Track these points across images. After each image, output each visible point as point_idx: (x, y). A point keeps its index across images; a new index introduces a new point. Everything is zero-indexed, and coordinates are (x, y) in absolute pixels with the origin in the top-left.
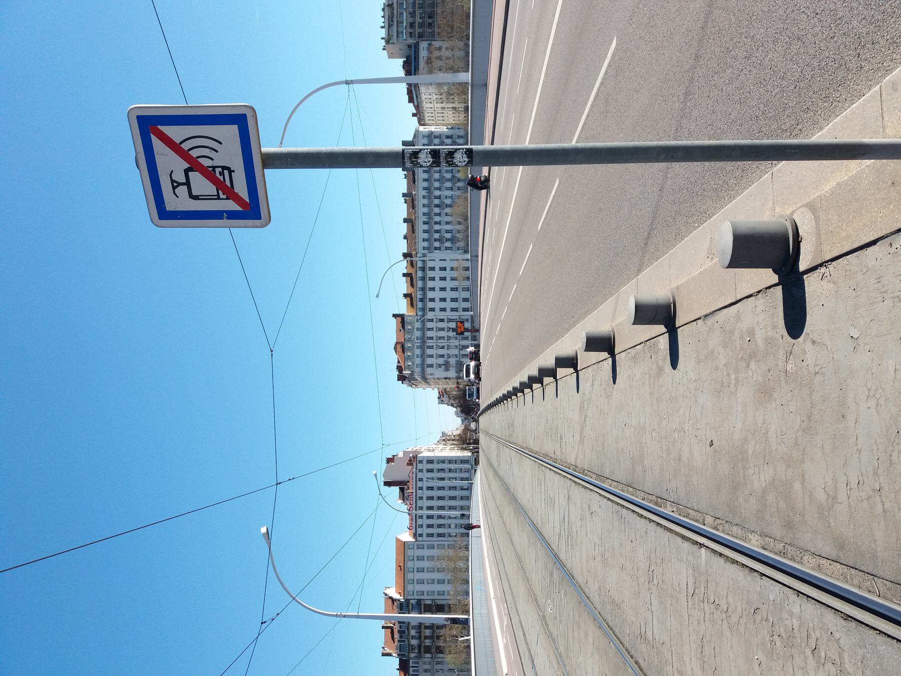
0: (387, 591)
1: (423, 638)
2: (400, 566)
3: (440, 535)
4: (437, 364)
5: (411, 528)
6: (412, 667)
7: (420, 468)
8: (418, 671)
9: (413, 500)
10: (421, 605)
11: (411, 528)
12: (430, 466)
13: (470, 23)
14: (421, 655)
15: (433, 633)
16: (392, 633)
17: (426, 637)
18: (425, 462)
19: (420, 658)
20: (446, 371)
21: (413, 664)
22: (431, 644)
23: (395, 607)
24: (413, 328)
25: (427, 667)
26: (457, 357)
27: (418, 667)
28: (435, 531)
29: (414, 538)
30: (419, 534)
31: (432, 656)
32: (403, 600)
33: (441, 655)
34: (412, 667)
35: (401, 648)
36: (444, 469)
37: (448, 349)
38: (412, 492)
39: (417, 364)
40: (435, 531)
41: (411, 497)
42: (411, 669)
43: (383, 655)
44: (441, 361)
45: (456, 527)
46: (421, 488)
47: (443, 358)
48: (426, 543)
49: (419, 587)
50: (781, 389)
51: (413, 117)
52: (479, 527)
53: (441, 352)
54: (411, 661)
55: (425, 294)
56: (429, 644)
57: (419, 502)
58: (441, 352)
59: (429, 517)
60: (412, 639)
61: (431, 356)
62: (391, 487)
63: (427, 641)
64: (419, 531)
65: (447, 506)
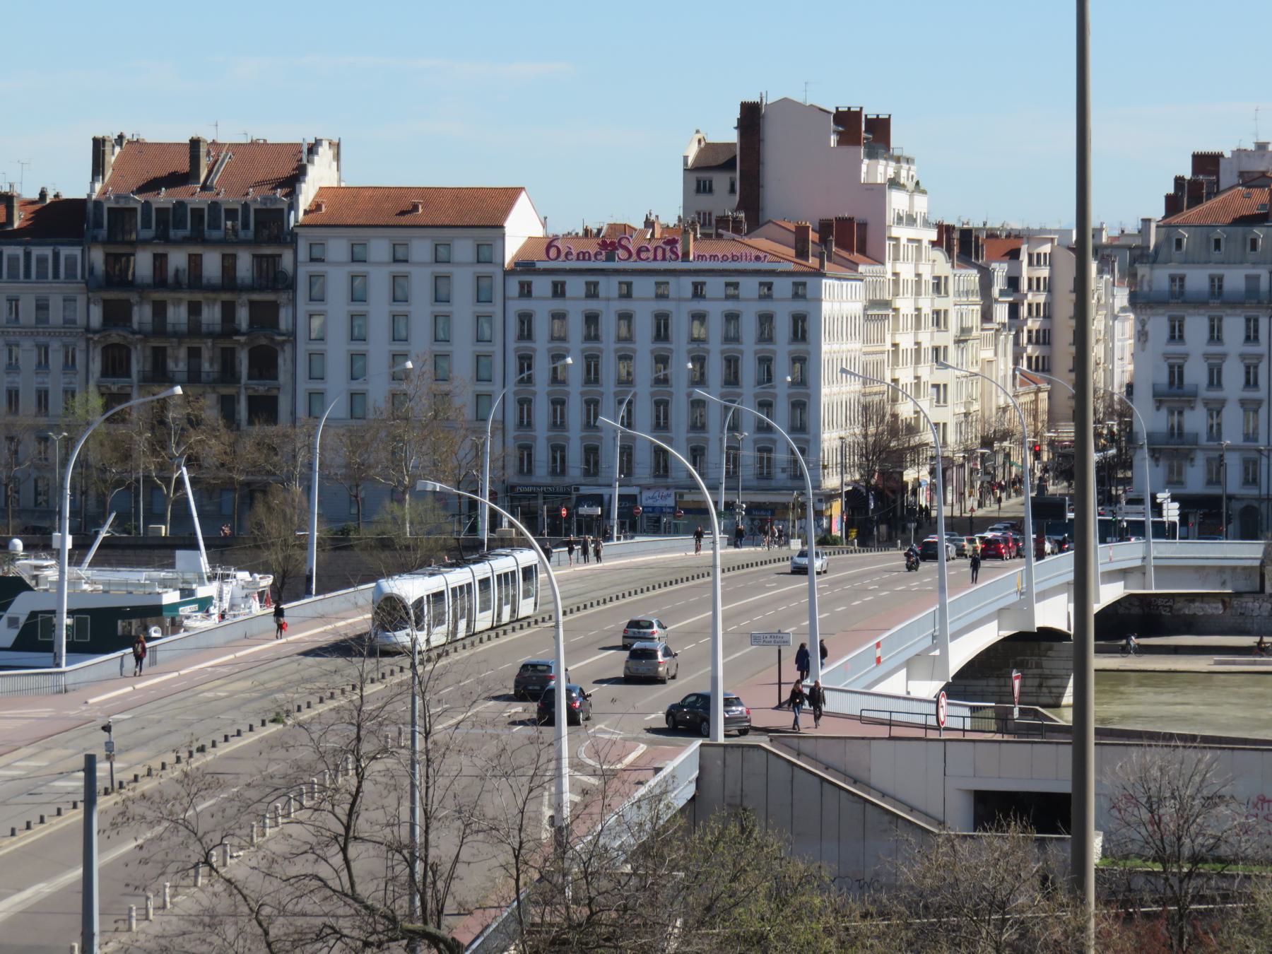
0: (325, 152)
1: (157, 296)
2: (415, 208)
3: (526, 362)
4: (1185, 356)
5: (553, 252)
6: (56, 256)
8: (42, 275)
9: (655, 259)
10: (275, 289)
11: (553, 252)
12: (783, 328)
14: (100, 288)
15: (176, 334)
16: (175, 180)
17: (160, 309)
18: (799, 306)
19: (87, 284)
20: (1154, 396)
21: (67, 258)
22: (135, 326)
23: (266, 191)
24: (1186, 262)
25: (56, 315)
26: (1210, 438)
27: (56, 275)
28: (749, 349)
29: (517, 264)
30: (563, 284)
31: (95, 332)
32: (292, 224)
33: (96, 366)
34: (56, 256)
35: (120, 216)
36: (769, 380)
37: (1243, 403)
38: (686, 255)
41: (668, 254)
42: (48, 251)
43: (99, 144)
44: (1196, 374)
46: (698, 291)
48: (497, 309)
49: (337, 281)
50: (217, 872)
52: (697, 549)
53: (1233, 374)
54: (77, 251)
55: (1198, 303)
56: (135, 318)
57: (687, 282)
58: (1233, 374)
59: (766, 320)
61: (1215, 336)
64: (542, 286)
65: (671, 394)
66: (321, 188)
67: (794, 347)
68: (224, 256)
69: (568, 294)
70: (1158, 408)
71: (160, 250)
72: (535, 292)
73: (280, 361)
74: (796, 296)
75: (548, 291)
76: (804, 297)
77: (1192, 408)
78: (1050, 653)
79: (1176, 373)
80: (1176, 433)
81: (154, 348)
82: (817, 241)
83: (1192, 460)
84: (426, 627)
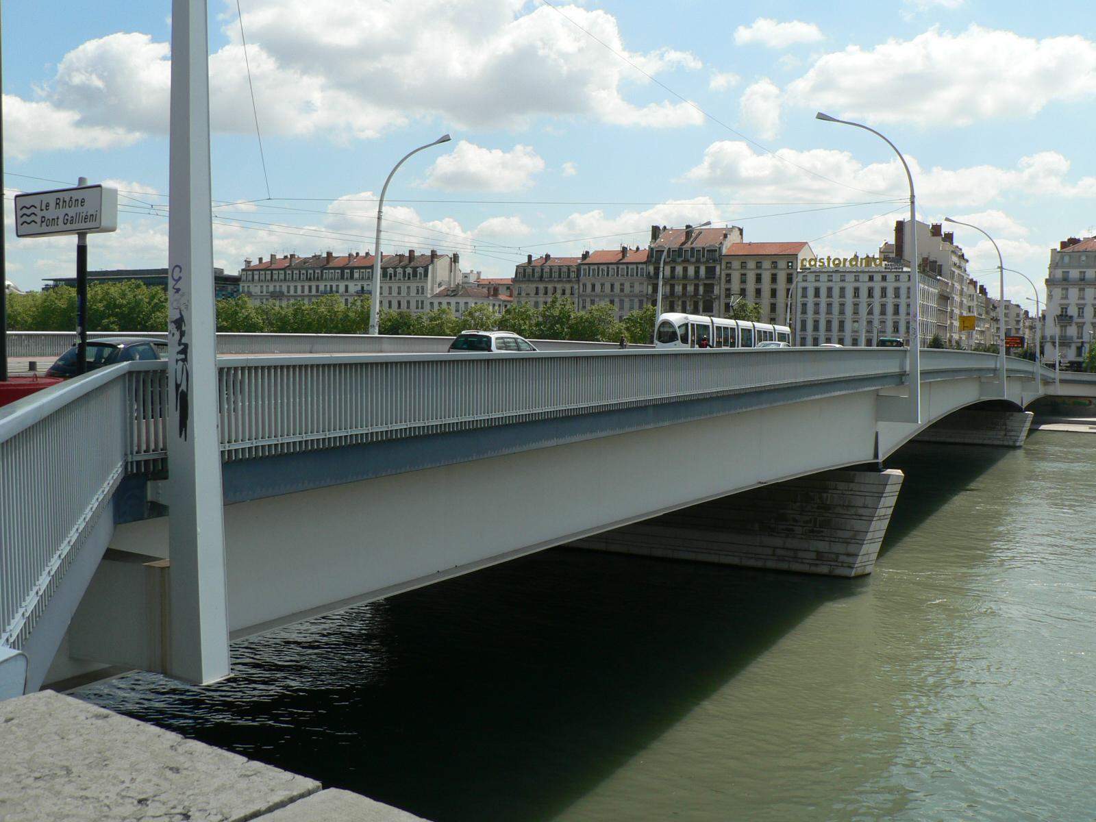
4: (1068, 305)
7: (901, 277)
13: (240, 332)
18: (909, 284)
25: (627, 289)
26: (642, 300)
27: (637, 275)
39: (1068, 272)
40: (811, 299)
44: (1072, 311)
45: (855, 331)
47: (1077, 314)
59: (857, 290)
62: (894, 232)
63: (681, 287)
66: (517, 266)
67: (868, 300)
68: (695, 267)
71: (673, 265)
73: (714, 305)
75: (880, 278)
77: (1071, 326)
78: (1011, 418)
79: (1064, 309)
81: (670, 301)
83: (1070, 346)
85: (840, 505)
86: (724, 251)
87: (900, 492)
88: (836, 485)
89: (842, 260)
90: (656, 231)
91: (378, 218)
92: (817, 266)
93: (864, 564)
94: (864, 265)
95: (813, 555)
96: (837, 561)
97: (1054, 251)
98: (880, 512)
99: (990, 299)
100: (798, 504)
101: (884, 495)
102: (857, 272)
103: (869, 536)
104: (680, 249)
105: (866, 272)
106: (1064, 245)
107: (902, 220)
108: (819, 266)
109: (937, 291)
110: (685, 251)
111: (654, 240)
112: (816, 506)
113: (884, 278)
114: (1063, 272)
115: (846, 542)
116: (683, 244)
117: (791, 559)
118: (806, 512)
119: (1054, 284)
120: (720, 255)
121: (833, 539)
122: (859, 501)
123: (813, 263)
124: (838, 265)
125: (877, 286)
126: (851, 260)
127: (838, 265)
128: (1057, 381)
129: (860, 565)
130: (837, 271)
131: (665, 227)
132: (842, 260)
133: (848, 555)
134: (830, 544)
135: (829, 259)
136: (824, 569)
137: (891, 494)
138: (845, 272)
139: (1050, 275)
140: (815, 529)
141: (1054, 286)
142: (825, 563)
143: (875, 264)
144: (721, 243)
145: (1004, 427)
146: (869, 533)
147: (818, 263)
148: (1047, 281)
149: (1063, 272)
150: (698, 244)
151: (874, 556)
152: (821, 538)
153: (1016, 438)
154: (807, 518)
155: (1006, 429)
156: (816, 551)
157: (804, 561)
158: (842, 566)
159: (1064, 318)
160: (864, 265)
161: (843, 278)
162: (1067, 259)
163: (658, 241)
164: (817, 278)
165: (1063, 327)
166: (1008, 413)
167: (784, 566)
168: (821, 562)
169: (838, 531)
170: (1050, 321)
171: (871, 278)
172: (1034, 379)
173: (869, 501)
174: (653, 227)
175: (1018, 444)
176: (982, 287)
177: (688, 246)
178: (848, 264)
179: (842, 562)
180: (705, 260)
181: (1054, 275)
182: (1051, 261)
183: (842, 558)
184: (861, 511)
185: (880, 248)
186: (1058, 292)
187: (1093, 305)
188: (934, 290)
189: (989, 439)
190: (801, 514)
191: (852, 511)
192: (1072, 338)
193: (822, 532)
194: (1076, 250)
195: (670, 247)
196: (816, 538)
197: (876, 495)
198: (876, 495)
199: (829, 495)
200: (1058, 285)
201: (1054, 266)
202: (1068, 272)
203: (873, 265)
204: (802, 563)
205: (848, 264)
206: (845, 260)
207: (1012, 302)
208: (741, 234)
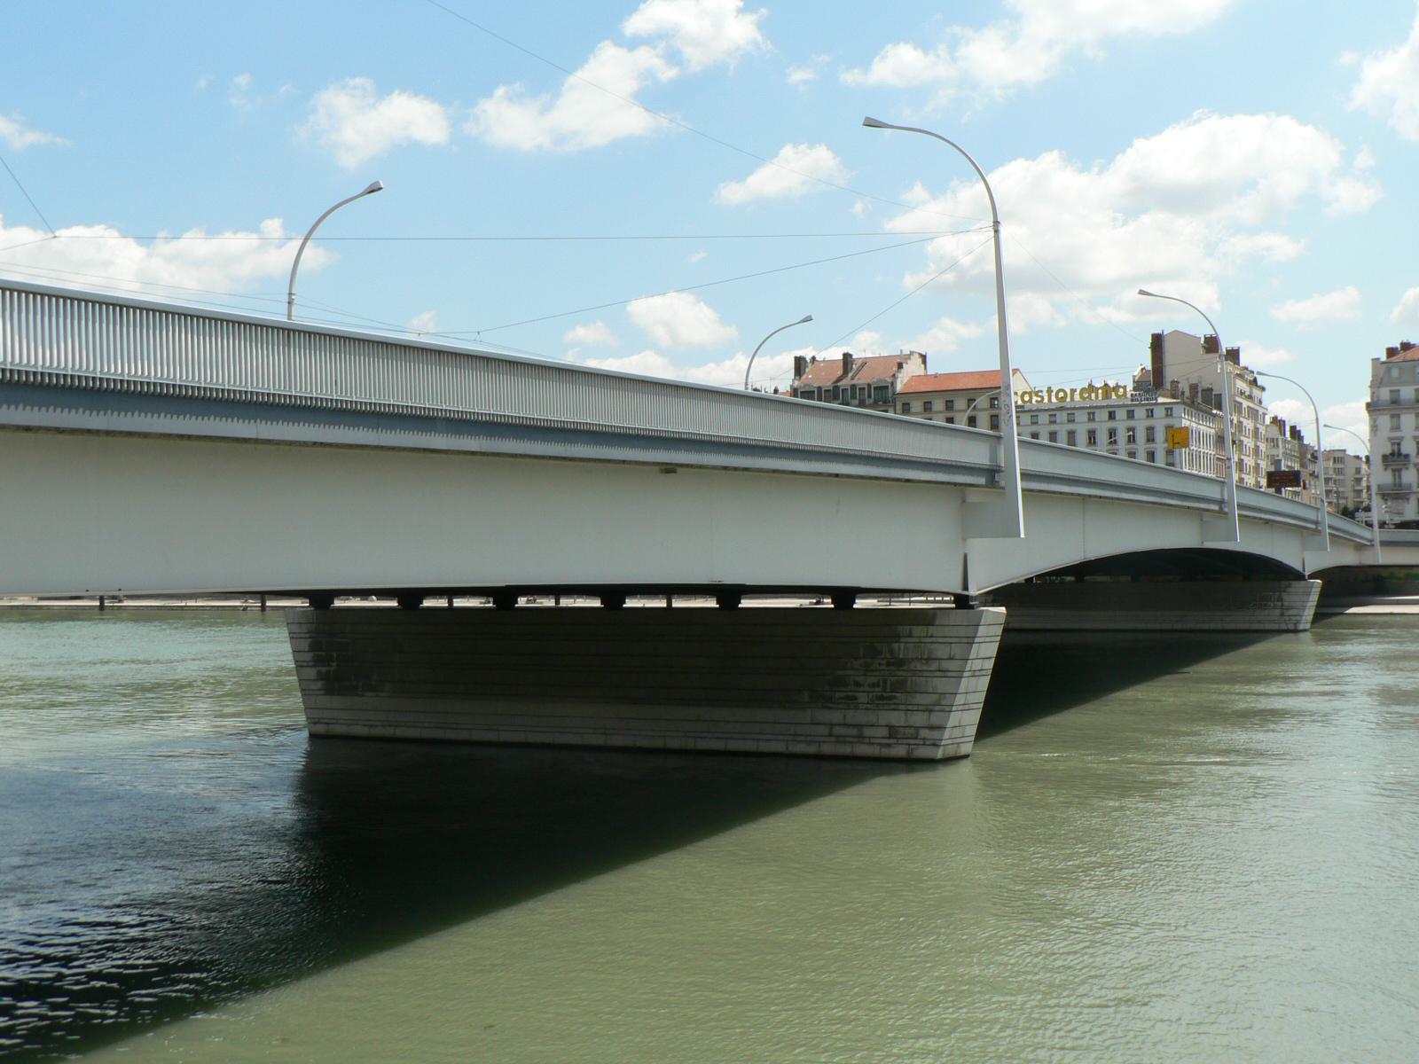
4: (1402, 438)
39: (1399, 391)
51: (793, 359)
57: (1064, 414)
60: (1068, 414)
62: (1150, 350)
69: (1174, 415)
70: (1386, 469)
72: (913, 410)
74: (992, 406)
76: (1037, 423)
77: (1407, 469)
78: (1289, 590)
80: (1398, 485)
82: (1136, 379)
83: (1408, 499)
84: (1137, 734)
85: (917, 658)
86: (899, 387)
87: (1002, 636)
88: (910, 630)
89: (1069, 392)
90: (800, 364)
91: (289, 303)
92: (1034, 402)
93: (955, 741)
94: (1100, 398)
95: (884, 732)
96: (916, 738)
97: (1375, 361)
98: (975, 664)
99: (1307, 446)
100: (861, 661)
101: (976, 640)
102: (1090, 407)
103: (960, 699)
104: (836, 388)
105: (1103, 407)
106: (1391, 352)
107: (1160, 332)
108: (1036, 401)
109: (1213, 431)
110: (843, 390)
111: (797, 378)
112: (884, 662)
113: (1131, 415)
114: (1391, 391)
115: (929, 710)
116: (839, 380)
117: (855, 740)
118: (873, 671)
119: (1379, 410)
120: (894, 394)
121: (910, 707)
122: (942, 651)
123: (1027, 398)
124: (1063, 399)
125: (1121, 425)
126: (1083, 390)
127: (1063, 399)
128: (1377, 543)
129: (950, 742)
130: (1062, 409)
131: (814, 358)
132: (1069, 392)
133: (932, 728)
134: (906, 715)
135: (1050, 391)
136: (900, 751)
137: (987, 639)
138: (1075, 408)
139: (1372, 397)
140: (885, 694)
141: (1378, 413)
142: (900, 741)
143: (1117, 395)
144: (894, 375)
145: (1280, 604)
146: (958, 695)
147: (1035, 399)
148: (1368, 405)
149: (1391, 391)
150: (861, 380)
151: (972, 730)
152: (893, 707)
153: (1298, 618)
154: (873, 680)
155: (1282, 606)
156: (887, 726)
157: (872, 741)
158: (924, 744)
159: (1395, 459)
160: (1100, 398)
161: (1071, 418)
162: (1395, 373)
163: (804, 377)
164: (1034, 420)
165: (1397, 472)
166: (1284, 583)
167: (845, 750)
168: (895, 741)
169: (918, 695)
170: (1377, 462)
171: (1112, 416)
172: (1317, 532)
173: (957, 650)
174: (796, 358)
175: (1301, 627)
176: (1293, 429)
177: (845, 383)
178: (1077, 397)
179: (924, 739)
180: (872, 401)
181: (1378, 397)
182: (1373, 376)
183: (924, 733)
184: (946, 665)
185: (1134, 376)
186: (1385, 421)
187: (1415, 437)
188: (1209, 430)
189: (1259, 622)
190: (865, 675)
191: (934, 666)
192: (1410, 486)
193: (895, 698)
194: (1408, 358)
195: (821, 385)
196: (886, 707)
197: (966, 640)
198: (966, 640)
199: (902, 645)
200: (1384, 410)
201: (1376, 384)
202: (1399, 391)
203: (1114, 397)
204: (870, 744)
205: (1077, 397)
206: (1073, 391)
207: (1348, 453)
208: (924, 362)
